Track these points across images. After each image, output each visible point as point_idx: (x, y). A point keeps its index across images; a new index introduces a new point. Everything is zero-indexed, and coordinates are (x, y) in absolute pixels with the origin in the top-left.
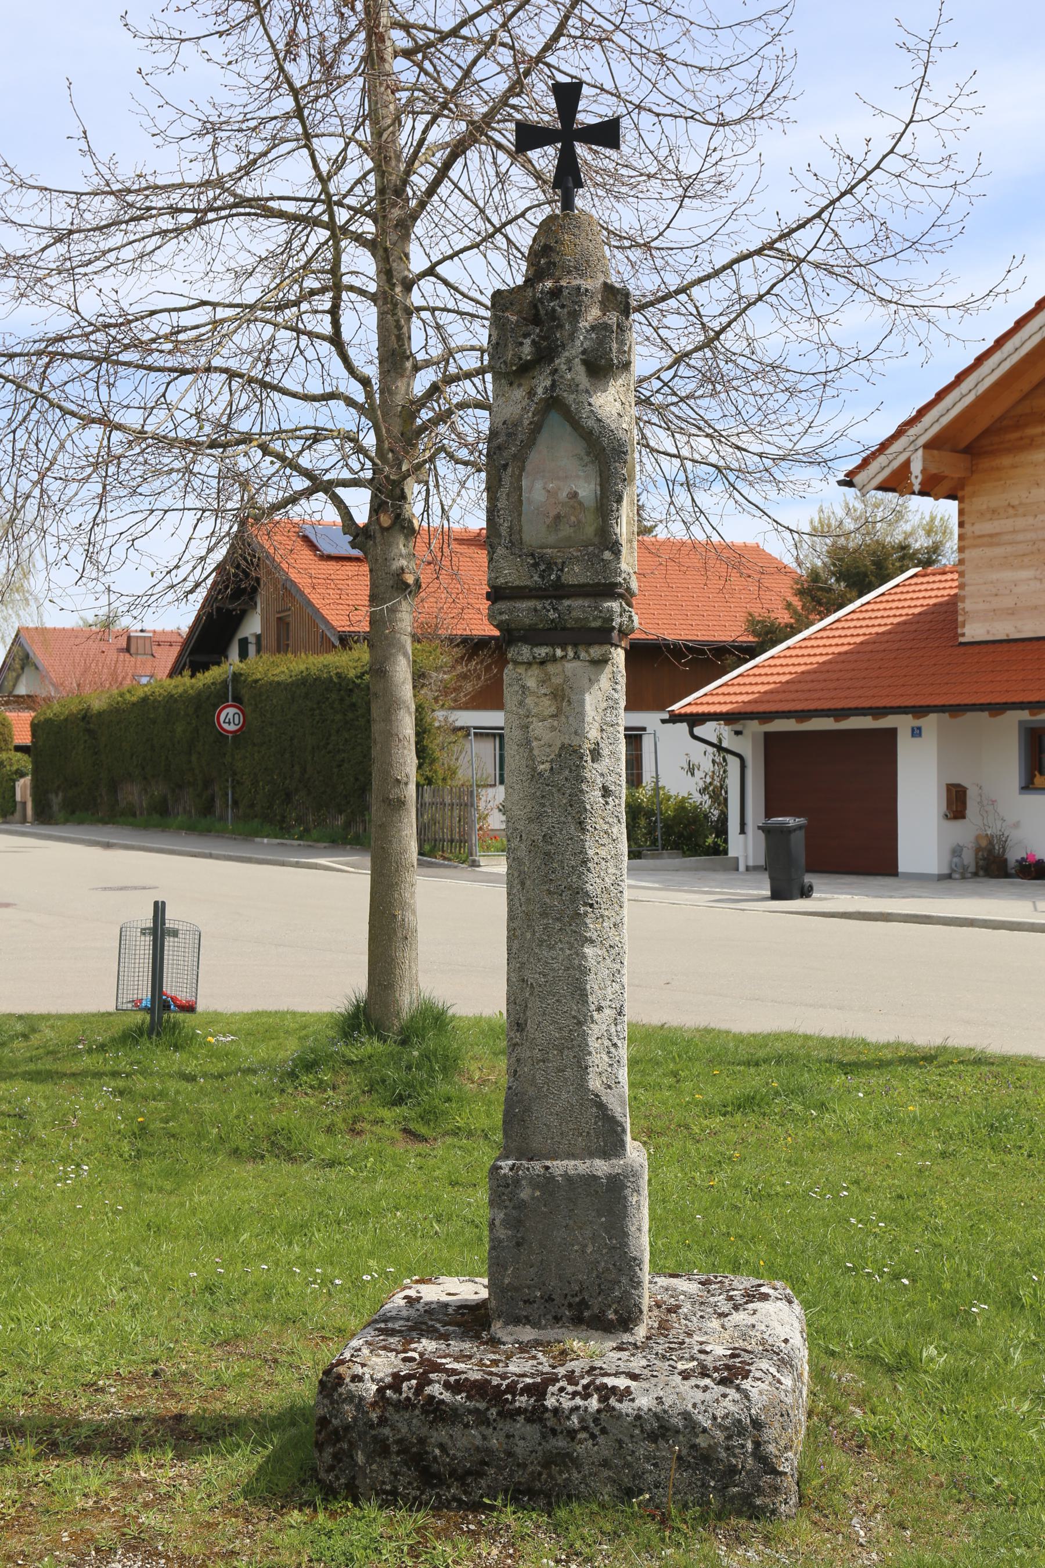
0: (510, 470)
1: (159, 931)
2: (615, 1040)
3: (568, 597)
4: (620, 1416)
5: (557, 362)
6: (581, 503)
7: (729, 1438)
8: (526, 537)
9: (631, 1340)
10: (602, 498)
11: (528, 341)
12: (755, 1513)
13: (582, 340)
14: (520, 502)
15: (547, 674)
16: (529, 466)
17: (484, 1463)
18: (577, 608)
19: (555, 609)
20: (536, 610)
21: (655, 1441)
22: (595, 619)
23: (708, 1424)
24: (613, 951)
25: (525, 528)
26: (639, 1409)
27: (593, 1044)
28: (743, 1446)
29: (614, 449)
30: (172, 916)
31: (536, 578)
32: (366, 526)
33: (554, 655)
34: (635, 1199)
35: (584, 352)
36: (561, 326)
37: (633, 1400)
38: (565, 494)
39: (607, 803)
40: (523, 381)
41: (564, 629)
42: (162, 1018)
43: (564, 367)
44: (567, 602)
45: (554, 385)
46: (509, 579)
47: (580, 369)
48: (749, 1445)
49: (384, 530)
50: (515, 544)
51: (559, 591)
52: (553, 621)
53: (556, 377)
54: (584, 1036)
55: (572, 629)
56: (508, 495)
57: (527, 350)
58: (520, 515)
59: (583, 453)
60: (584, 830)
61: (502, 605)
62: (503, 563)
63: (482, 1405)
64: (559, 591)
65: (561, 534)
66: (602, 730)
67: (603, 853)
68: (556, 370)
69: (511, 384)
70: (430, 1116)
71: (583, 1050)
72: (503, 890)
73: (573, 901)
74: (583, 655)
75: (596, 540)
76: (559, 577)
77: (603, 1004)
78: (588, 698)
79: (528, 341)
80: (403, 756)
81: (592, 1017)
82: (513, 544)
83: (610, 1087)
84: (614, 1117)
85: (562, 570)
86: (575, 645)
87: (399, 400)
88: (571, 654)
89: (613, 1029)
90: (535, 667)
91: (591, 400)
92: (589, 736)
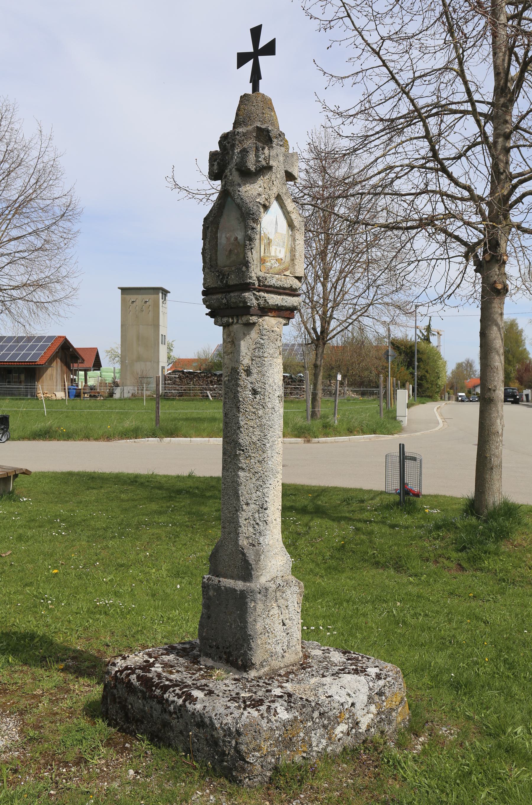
1: (403, 457)
2: (258, 521)
4: (187, 711)
6: (239, 243)
7: (225, 736)
9: (247, 677)
12: (233, 780)
14: (217, 245)
17: (143, 717)
21: (199, 728)
23: (218, 726)
24: (257, 475)
26: (195, 709)
27: (242, 521)
28: (230, 742)
30: (408, 451)
34: (253, 604)
35: (236, 165)
36: (228, 153)
37: (195, 704)
39: (255, 398)
42: (406, 498)
43: (229, 174)
47: (235, 174)
48: (233, 742)
54: (238, 517)
58: (216, 251)
60: (239, 411)
63: (145, 690)
66: (252, 360)
67: (251, 423)
70: (474, 560)
71: (237, 525)
72: (477, 447)
73: (235, 448)
76: (227, 281)
77: (250, 502)
78: (242, 343)
80: (494, 376)
81: (242, 508)
83: (254, 545)
84: (248, 561)
88: (235, 321)
89: (257, 515)
91: (240, 189)
92: (243, 362)
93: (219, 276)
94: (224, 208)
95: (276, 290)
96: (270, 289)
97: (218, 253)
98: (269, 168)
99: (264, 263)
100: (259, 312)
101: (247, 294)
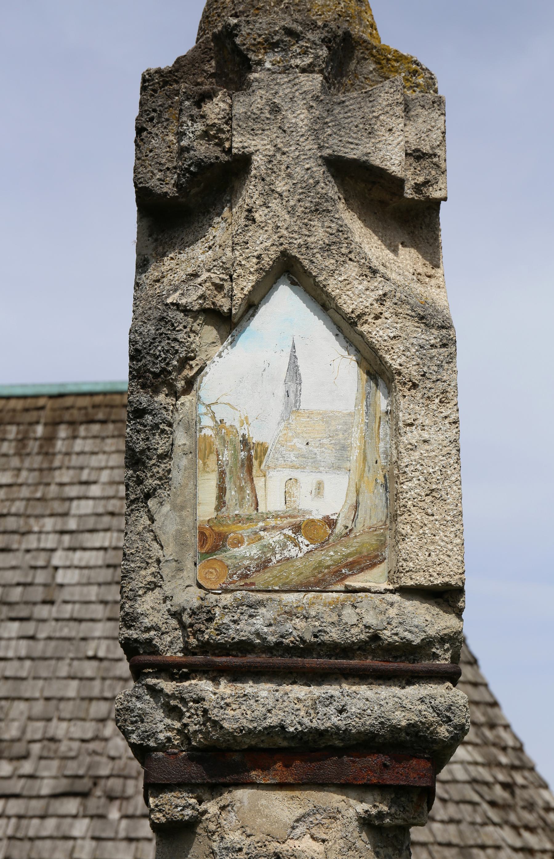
95: (287, 660)
96: (251, 658)
98: (241, 164)
99: (215, 549)
100: (195, 771)
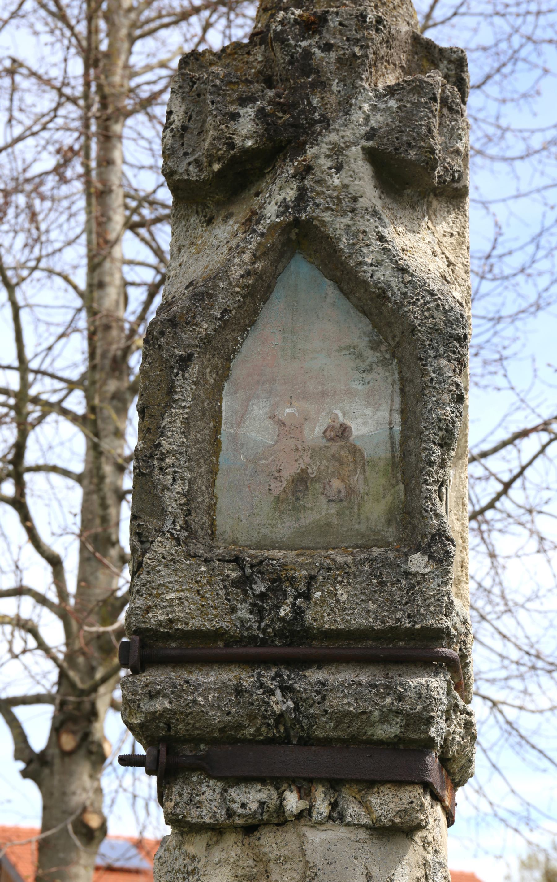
0: (194, 369)
3: (320, 662)
5: (311, 152)
6: (355, 451)
8: (224, 523)
10: (405, 438)
11: (248, 112)
13: (368, 110)
14: (216, 444)
15: (260, 859)
16: (240, 368)
18: (342, 687)
19: (286, 690)
20: (239, 691)
22: (384, 719)
25: (223, 503)
29: (435, 329)
31: (243, 613)
32: (43, 753)
33: (281, 808)
35: (371, 135)
36: (322, 85)
38: (318, 430)
40: (233, 209)
41: (307, 741)
43: (325, 163)
44: (315, 676)
45: (302, 197)
46: (179, 612)
47: (361, 179)
49: (66, 754)
50: (197, 530)
51: (298, 647)
52: (280, 718)
53: (307, 183)
55: (326, 742)
56: (186, 422)
57: (246, 128)
58: (213, 472)
59: (363, 344)
61: (158, 677)
62: (165, 575)
64: (298, 647)
65: (308, 518)
68: (309, 169)
69: (210, 221)
74: (353, 810)
75: (391, 534)
76: (299, 613)
79: (248, 112)
82: (192, 534)
85: (307, 596)
86: (334, 784)
87: (99, 592)
88: (322, 807)
90: (231, 839)
93: (244, 583)
94: (265, 299)
97: (220, 481)
101: (417, 681)
